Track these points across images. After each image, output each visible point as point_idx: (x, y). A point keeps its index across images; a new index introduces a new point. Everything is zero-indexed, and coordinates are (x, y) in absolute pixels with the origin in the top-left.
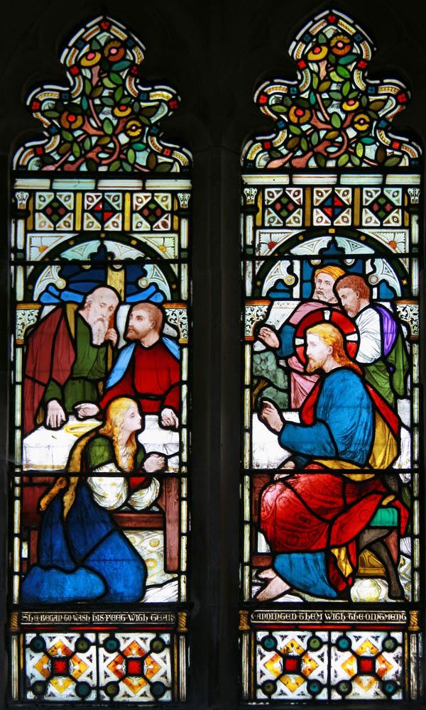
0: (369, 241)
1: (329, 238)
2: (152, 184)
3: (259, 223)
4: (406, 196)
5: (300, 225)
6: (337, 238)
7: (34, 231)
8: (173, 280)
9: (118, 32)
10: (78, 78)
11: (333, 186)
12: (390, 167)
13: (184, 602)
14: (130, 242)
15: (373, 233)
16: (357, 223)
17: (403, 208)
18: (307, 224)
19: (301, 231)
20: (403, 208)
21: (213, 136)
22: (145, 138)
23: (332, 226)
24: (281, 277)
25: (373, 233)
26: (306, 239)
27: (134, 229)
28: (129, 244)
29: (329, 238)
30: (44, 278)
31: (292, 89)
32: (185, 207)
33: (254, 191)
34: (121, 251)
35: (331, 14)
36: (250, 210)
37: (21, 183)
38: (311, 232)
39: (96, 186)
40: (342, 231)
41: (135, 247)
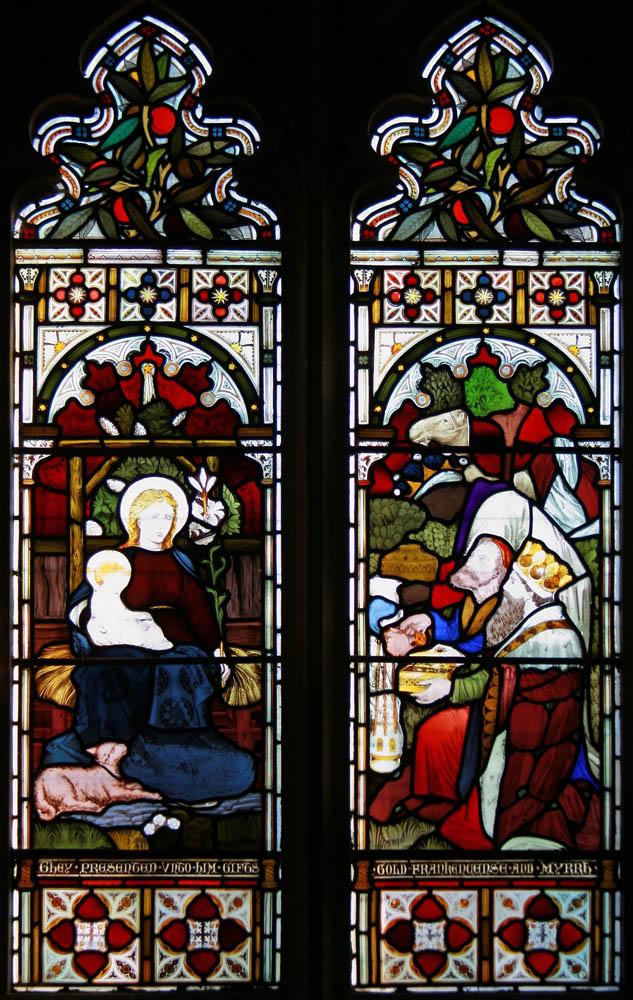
0: (204, 343)
1: (142, 339)
2: (218, 255)
3: (41, 316)
4: (591, 283)
5: (102, 319)
6: (152, 338)
7: (47, 322)
8: (589, 401)
9: (127, 44)
10: (108, 111)
11: (77, 266)
12: (60, 240)
13: (362, 851)
14: (536, 342)
15: (212, 332)
16: (521, 319)
17: (251, 296)
18: (448, 321)
19: (101, 328)
20: (587, 296)
21: (315, 195)
22: (158, 200)
23: (485, 325)
24: (552, 389)
25: (212, 332)
26: (108, 340)
27: (531, 322)
28: (525, 342)
29: (142, 339)
30: (64, 391)
31: (555, 129)
32: (604, 292)
33: (34, 272)
34: (511, 353)
35: (485, 23)
36: (268, 299)
37: (23, 255)
38: (450, 331)
39: (541, 260)
40: (497, 331)
41: (535, 347)
